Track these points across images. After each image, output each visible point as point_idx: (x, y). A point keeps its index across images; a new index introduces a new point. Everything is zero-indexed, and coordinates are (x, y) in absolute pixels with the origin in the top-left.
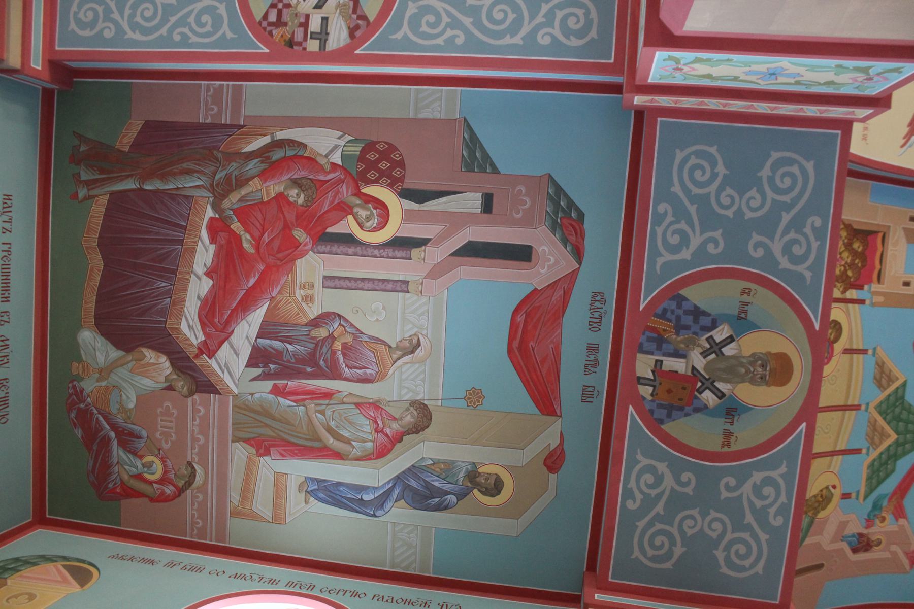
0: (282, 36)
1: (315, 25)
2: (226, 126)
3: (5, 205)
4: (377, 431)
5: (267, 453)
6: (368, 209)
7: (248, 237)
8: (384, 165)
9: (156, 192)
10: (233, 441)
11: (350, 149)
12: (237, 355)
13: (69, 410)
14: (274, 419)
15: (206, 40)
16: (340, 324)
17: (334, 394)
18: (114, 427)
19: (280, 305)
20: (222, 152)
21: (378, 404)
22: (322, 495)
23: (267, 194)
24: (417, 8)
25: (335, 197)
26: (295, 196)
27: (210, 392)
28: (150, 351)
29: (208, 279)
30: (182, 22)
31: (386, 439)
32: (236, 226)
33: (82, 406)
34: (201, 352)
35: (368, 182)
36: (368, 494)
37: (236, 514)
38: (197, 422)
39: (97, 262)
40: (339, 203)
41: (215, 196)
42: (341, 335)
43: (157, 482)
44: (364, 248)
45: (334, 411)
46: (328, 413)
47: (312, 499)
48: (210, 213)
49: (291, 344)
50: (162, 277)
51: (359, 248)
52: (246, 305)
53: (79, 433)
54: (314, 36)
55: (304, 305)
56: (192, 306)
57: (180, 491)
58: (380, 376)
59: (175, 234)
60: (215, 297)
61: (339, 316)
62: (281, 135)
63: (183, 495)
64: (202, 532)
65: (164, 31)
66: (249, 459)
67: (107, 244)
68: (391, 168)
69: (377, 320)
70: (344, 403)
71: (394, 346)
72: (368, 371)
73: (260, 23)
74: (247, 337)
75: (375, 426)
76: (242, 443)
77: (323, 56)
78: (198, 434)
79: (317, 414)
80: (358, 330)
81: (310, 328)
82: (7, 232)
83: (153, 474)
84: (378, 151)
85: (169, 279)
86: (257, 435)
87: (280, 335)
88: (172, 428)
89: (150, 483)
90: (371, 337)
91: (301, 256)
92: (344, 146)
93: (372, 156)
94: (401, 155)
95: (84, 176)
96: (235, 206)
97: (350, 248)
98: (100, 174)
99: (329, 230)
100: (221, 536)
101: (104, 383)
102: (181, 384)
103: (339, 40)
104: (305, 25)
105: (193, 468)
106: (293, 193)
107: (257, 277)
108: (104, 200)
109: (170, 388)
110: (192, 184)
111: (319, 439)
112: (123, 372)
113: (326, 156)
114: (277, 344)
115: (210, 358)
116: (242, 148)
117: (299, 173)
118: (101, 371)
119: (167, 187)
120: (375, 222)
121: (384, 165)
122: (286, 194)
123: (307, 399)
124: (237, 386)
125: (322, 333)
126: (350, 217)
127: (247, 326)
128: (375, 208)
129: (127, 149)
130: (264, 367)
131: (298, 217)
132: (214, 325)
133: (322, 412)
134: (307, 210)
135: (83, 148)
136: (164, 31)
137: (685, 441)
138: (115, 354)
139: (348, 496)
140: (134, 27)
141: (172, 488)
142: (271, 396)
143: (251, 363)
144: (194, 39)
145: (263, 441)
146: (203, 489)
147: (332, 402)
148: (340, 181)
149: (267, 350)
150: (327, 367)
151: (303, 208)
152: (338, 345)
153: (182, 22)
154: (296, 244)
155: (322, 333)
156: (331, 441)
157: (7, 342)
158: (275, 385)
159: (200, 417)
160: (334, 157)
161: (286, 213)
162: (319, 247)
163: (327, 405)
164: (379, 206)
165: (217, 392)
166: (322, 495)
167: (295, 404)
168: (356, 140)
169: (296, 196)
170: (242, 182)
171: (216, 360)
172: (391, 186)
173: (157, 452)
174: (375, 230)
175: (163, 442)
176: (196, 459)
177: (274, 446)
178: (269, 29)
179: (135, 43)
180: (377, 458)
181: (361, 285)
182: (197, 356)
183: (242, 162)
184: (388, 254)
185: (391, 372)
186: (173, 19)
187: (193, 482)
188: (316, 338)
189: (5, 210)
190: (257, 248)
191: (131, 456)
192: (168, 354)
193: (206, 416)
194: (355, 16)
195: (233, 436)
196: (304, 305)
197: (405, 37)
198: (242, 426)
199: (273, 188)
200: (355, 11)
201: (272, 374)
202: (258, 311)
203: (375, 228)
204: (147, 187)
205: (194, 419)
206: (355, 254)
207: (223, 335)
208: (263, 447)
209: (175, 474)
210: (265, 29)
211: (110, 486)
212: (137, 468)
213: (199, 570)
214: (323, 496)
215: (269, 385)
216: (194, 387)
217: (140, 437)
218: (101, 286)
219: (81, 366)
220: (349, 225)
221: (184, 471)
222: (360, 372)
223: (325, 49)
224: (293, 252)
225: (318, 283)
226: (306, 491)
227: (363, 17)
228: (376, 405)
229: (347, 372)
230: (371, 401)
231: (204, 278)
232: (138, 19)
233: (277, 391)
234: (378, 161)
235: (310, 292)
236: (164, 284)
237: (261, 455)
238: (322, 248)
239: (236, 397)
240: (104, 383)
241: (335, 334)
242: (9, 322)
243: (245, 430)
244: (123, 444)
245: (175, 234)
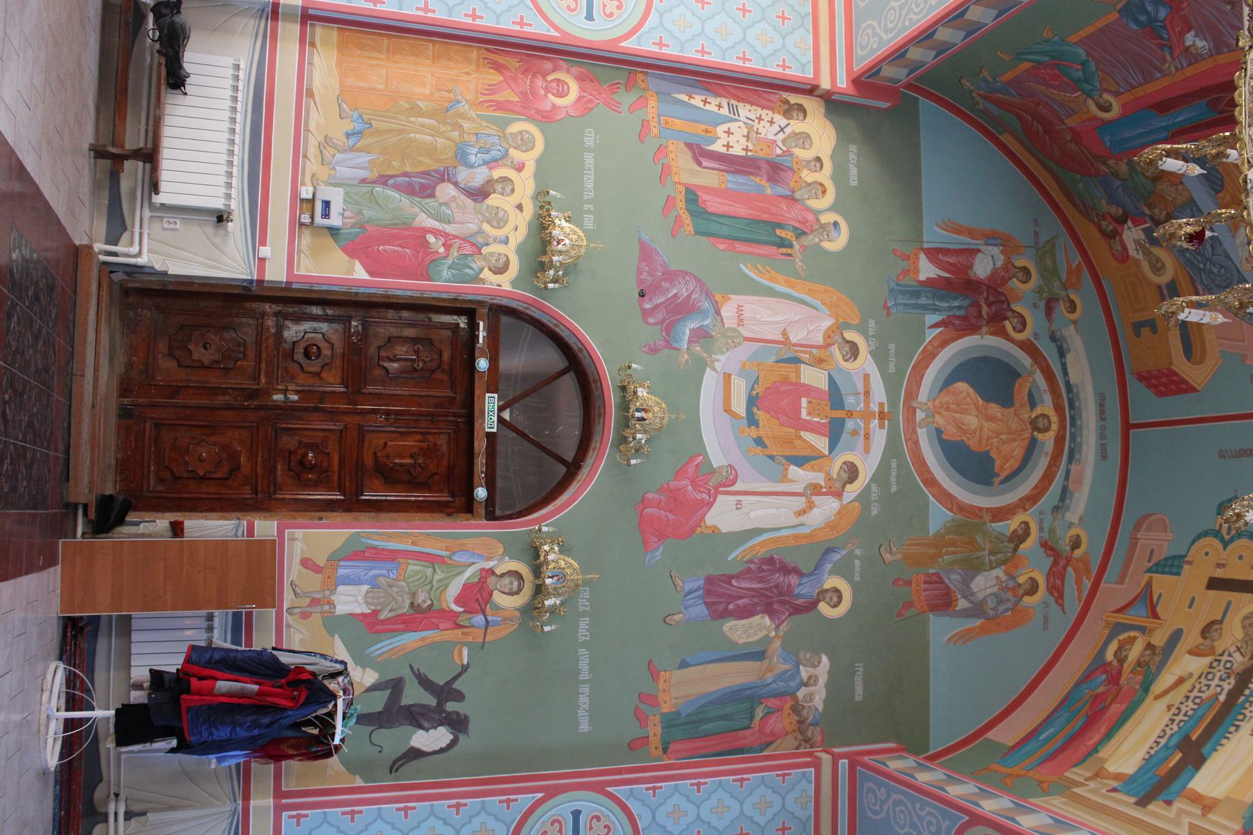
121: (1160, 569)
144: (916, 18)
153: (910, 10)
186: (904, 13)
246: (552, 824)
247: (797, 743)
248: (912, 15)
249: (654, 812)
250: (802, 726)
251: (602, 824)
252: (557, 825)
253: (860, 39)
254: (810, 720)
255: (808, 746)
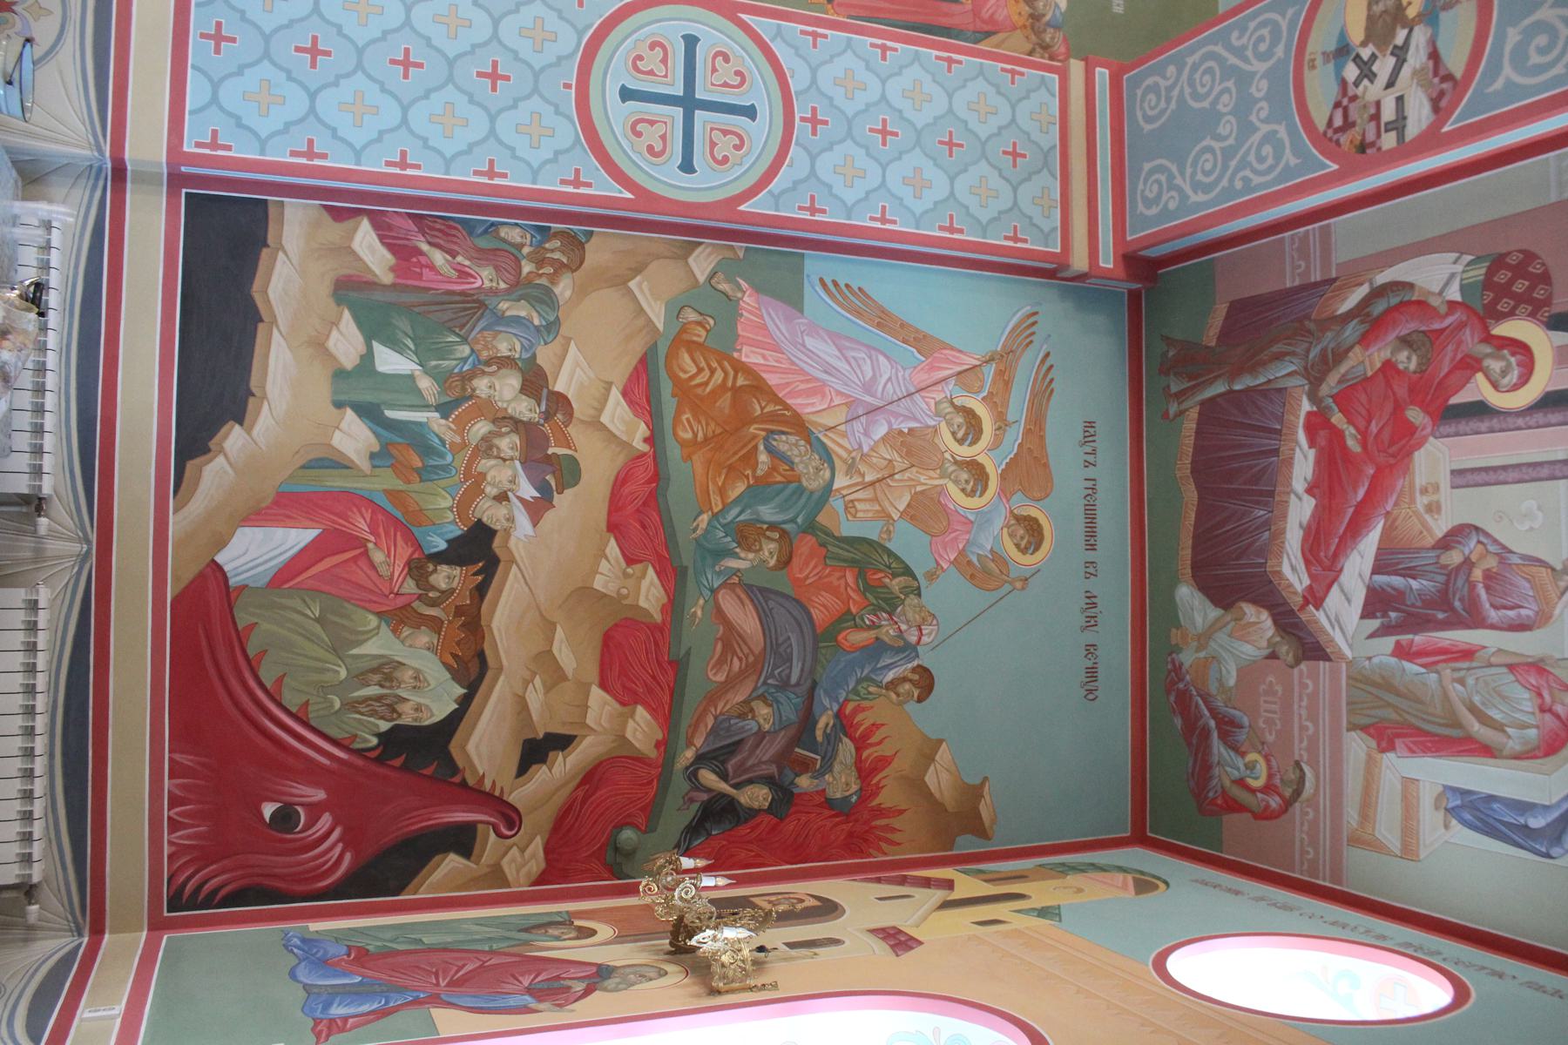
0: (1351, 142)
1: (1388, 113)
2: (1316, 285)
3: (1087, 434)
4: (1542, 710)
5: (1391, 747)
6: (1503, 358)
7: (1353, 431)
8: (1520, 286)
9: (1248, 391)
10: (1348, 730)
11: (1471, 274)
12: (1349, 601)
13: (1168, 692)
14: (1398, 694)
15: (1268, 178)
16: (1479, 542)
17: (1475, 651)
18: (1214, 712)
19: (1397, 524)
20: (1315, 320)
21: (1541, 664)
22: (1468, 816)
23: (1372, 364)
24: (1520, 33)
25: (1456, 350)
26: (1405, 360)
27: (1318, 658)
28: (1250, 605)
29: (1309, 497)
30: (1243, 164)
31: (1557, 723)
32: (1337, 419)
33: (1181, 686)
34: (1306, 602)
35: (1501, 317)
36: (1536, 817)
37: (1355, 841)
38: (1304, 703)
39: (1191, 494)
40: (1462, 359)
41: (1311, 383)
42: (1482, 557)
43: (1261, 791)
44: (1502, 418)
45: (1477, 679)
46: (1470, 681)
47: (1454, 822)
48: (1306, 406)
49: (1414, 578)
50: (1258, 503)
51: (1495, 420)
52: (1356, 529)
53: (1178, 722)
54: (1389, 127)
55: (1427, 517)
56: (1293, 538)
57: (1288, 804)
58: (1543, 618)
59: (1268, 443)
60: (1319, 523)
61: (1477, 529)
62: (1382, 278)
63: (1291, 810)
64: (1313, 871)
65: (1224, 183)
66: (1369, 756)
67: (1200, 470)
68: (1531, 288)
69: (1531, 529)
70: (1491, 665)
71: (1559, 567)
72: (1523, 612)
73: (1325, 134)
74: (1360, 575)
75: (1539, 701)
76: (1359, 732)
77: (1407, 151)
78: (1306, 720)
79: (1456, 685)
80: (1504, 547)
81: (1439, 552)
82: (1091, 467)
83: (1256, 778)
84: (1509, 267)
85: (1266, 504)
86: (1377, 720)
87: (1401, 566)
88: (1275, 713)
89: (1253, 791)
90: (1524, 557)
91: (1420, 445)
92: (1464, 272)
93: (1502, 277)
94: (1543, 264)
95: (1174, 389)
96: (1335, 391)
97: (1482, 421)
98: (1189, 381)
99: (1454, 400)
100: (1337, 875)
101: (1202, 655)
102: (1285, 651)
103: (1420, 121)
104: (1376, 117)
105: (1301, 770)
106: (1402, 356)
107: (1366, 487)
108: (1194, 414)
109: (1273, 656)
110: (1284, 372)
111: (1457, 724)
112: (1221, 637)
113: (1440, 293)
114: (1397, 581)
115: (1317, 609)
116: (1336, 311)
117: (1406, 327)
118: (1199, 637)
119: (1258, 382)
120: (1514, 376)
121: (1520, 286)
122: (1394, 359)
123: (1438, 662)
124: (1351, 646)
125: (1454, 558)
126: (1480, 376)
127: (1358, 558)
128: (1513, 354)
129: (1213, 344)
130: (1383, 617)
131: (1412, 390)
132: (1319, 562)
133: (1462, 682)
134: (1421, 378)
135: (1171, 354)
136: (1224, 183)
137: (51, 44)
138: (1214, 613)
139: (1505, 819)
140: (1197, 186)
141: (1277, 799)
142: (1394, 660)
143: (1367, 613)
144: (1257, 180)
145: (1386, 728)
146: (1313, 802)
147: (1474, 664)
148: (1461, 326)
149: (1383, 589)
150: (1464, 610)
151: (1418, 375)
152: (1477, 574)
153: (1243, 164)
154: (1411, 429)
155: (1454, 558)
156: (1476, 728)
157: (1094, 600)
158: (1398, 643)
159: (1308, 695)
160: (1450, 291)
161: (1395, 387)
162: (1441, 429)
163: (1468, 669)
164: (1517, 350)
165: (1327, 658)
166: (1468, 816)
167: (1423, 670)
168: (1478, 259)
169: (1408, 361)
170: (1340, 355)
171: (1325, 611)
172: (1532, 315)
173: (1260, 748)
174: (1515, 387)
175: (1267, 734)
176: (1305, 758)
177: (1399, 736)
178: (1335, 137)
179: (1199, 205)
180: (1547, 754)
181: (1502, 476)
182: (1302, 608)
183: (1339, 328)
184: (1537, 422)
185: (1557, 612)
186: (1233, 164)
187: (1302, 792)
188: (1448, 566)
189: (1087, 439)
190: (1364, 444)
191: (1232, 754)
192: (1269, 607)
193: (1316, 693)
194: (1436, 80)
195: (1349, 722)
196: (1427, 517)
197: (1509, 84)
198: (1360, 706)
199: (1378, 355)
200: (1436, 73)
201: (1394, 627)
202: (1371, 534)
203: (1515, 385)
204: (1237, 387)
205: (1301, 699)
206: (1492, 431)
207: (1332, 574)
208: (1385, 737)
209: (1282, 780)
210: (1330, 140)
211: (1211, 794)
212: (1238, 769)
213: (1237, 893)
214: (1471, 818)
215: (1389, 642)
216: (1300, 652)
217: (1241, 727)
218: (1196, 526)
219: (1179, 632)
220: (1479, 389)
221: (1292, 775)
222: (1511, 613)
223: (1404, 142)
224: (1408, 442)
225: (1445, 480)
226: (1446, 809)
227: (1449, 77)
228: (1538, 667)
229: (1493, 615)
230: (1530, 660)
231: (1306, 497)
232: (1200, 177)
233: (1401, 652)
234: (1511, 282)
235: (1435, 497)
236: (1262, 513)
237: (1383, 751)
238: (1444, 429)
239: (1350, 663)
240: (1202, 655)
241: (1474, 558)
242: (1096, 576)
243: (1365, 712)
244: (1224, 736)
245: (1268, 443)
246: (639, 134)
247: (1029, 47)
248: (1247, 173)
249: (814, 71)
250: (1037, 24)
251: (731, 152)
252: (639, 127)
253: (1143, 188)
254: (1047, 18)
255: (1047, 55)
